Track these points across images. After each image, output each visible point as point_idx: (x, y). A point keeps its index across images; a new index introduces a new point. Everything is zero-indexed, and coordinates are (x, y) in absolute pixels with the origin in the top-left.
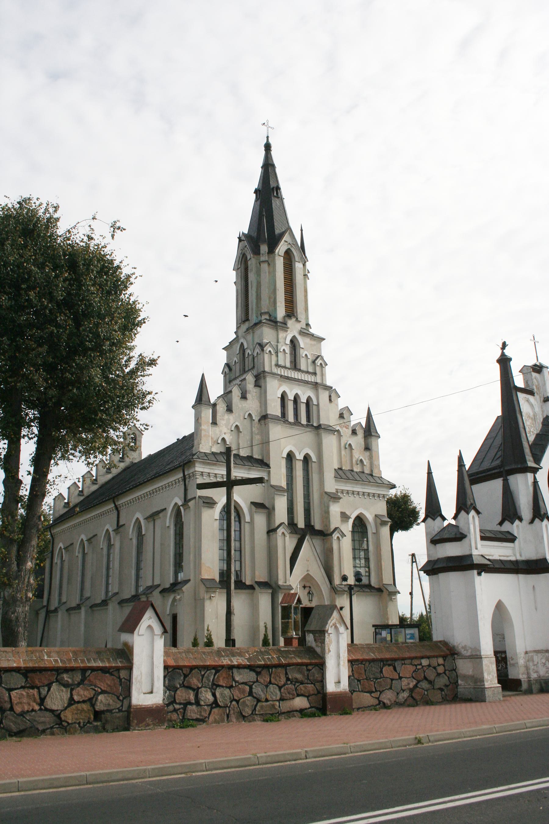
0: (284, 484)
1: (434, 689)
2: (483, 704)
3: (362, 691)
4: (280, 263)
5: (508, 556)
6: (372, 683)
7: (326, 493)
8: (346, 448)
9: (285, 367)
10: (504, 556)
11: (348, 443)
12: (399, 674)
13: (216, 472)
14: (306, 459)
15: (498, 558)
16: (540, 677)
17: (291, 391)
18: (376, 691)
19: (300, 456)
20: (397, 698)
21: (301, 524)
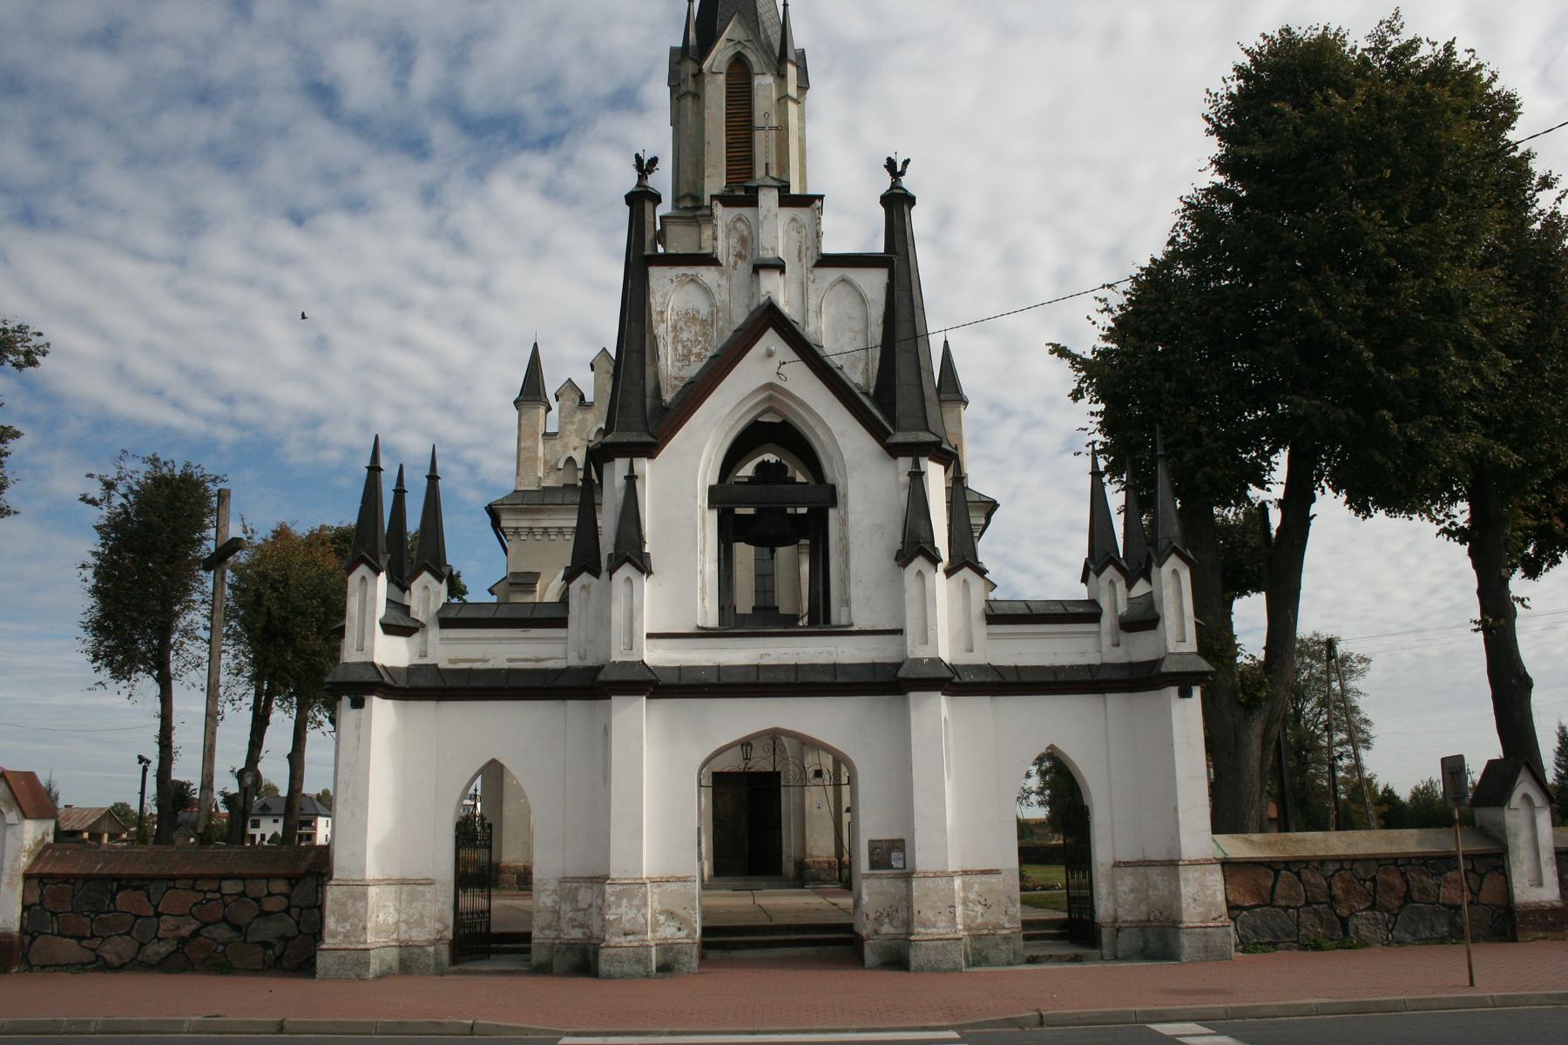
1: (245, 941)
2: (905, 974)
3: (59, 934)
6: (86, 920)
12: (156, 908)
13: (545, 524)
15: (506, 665)
16: (590, 937)
18: (93, 936)
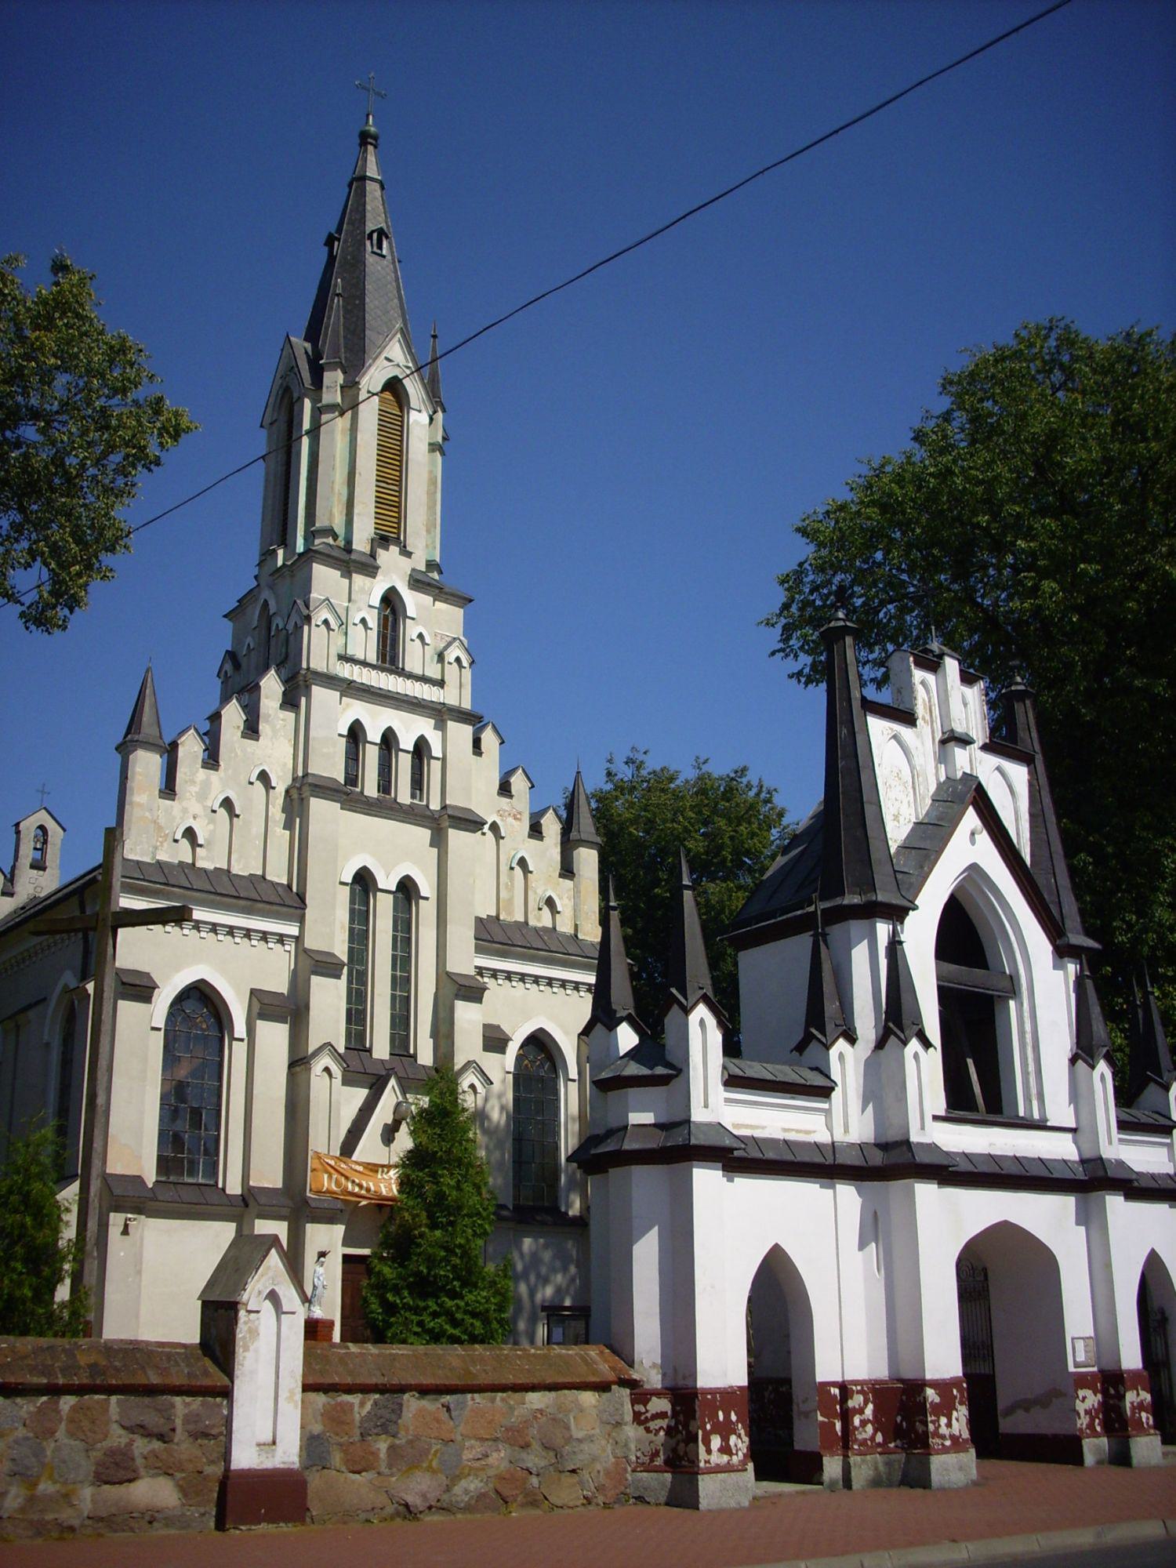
0: (341, 951)
4: (369, 413)
5: (807, 1132)
7: (448, 973)
8: (512, 868)
9: (364, 664)
10: (798, 1131)
11: (519, 856)
14: (407, 889)
15: (780, 1136)
17: (376, 720)
19: (387, 881)
20: (448, 1489)
21: (381, 1048)
